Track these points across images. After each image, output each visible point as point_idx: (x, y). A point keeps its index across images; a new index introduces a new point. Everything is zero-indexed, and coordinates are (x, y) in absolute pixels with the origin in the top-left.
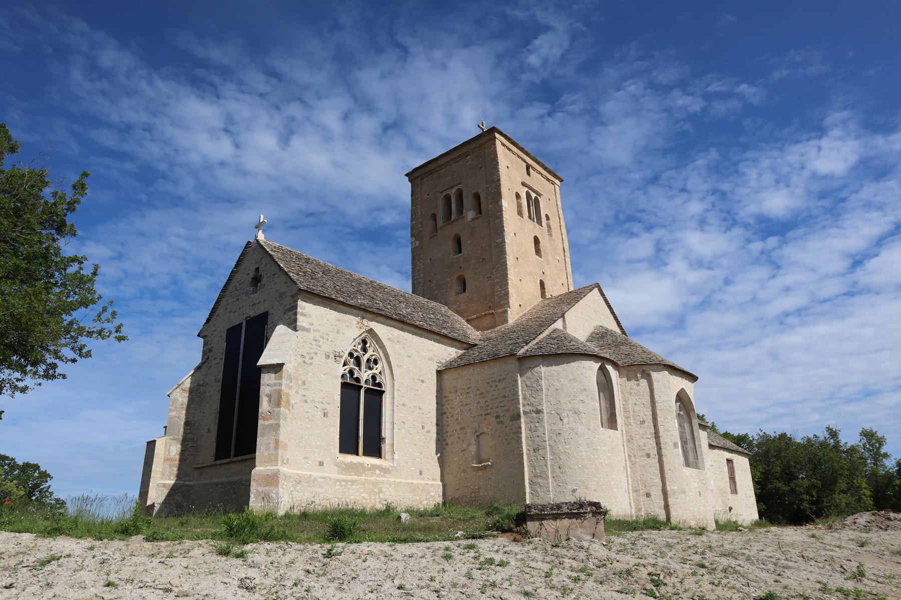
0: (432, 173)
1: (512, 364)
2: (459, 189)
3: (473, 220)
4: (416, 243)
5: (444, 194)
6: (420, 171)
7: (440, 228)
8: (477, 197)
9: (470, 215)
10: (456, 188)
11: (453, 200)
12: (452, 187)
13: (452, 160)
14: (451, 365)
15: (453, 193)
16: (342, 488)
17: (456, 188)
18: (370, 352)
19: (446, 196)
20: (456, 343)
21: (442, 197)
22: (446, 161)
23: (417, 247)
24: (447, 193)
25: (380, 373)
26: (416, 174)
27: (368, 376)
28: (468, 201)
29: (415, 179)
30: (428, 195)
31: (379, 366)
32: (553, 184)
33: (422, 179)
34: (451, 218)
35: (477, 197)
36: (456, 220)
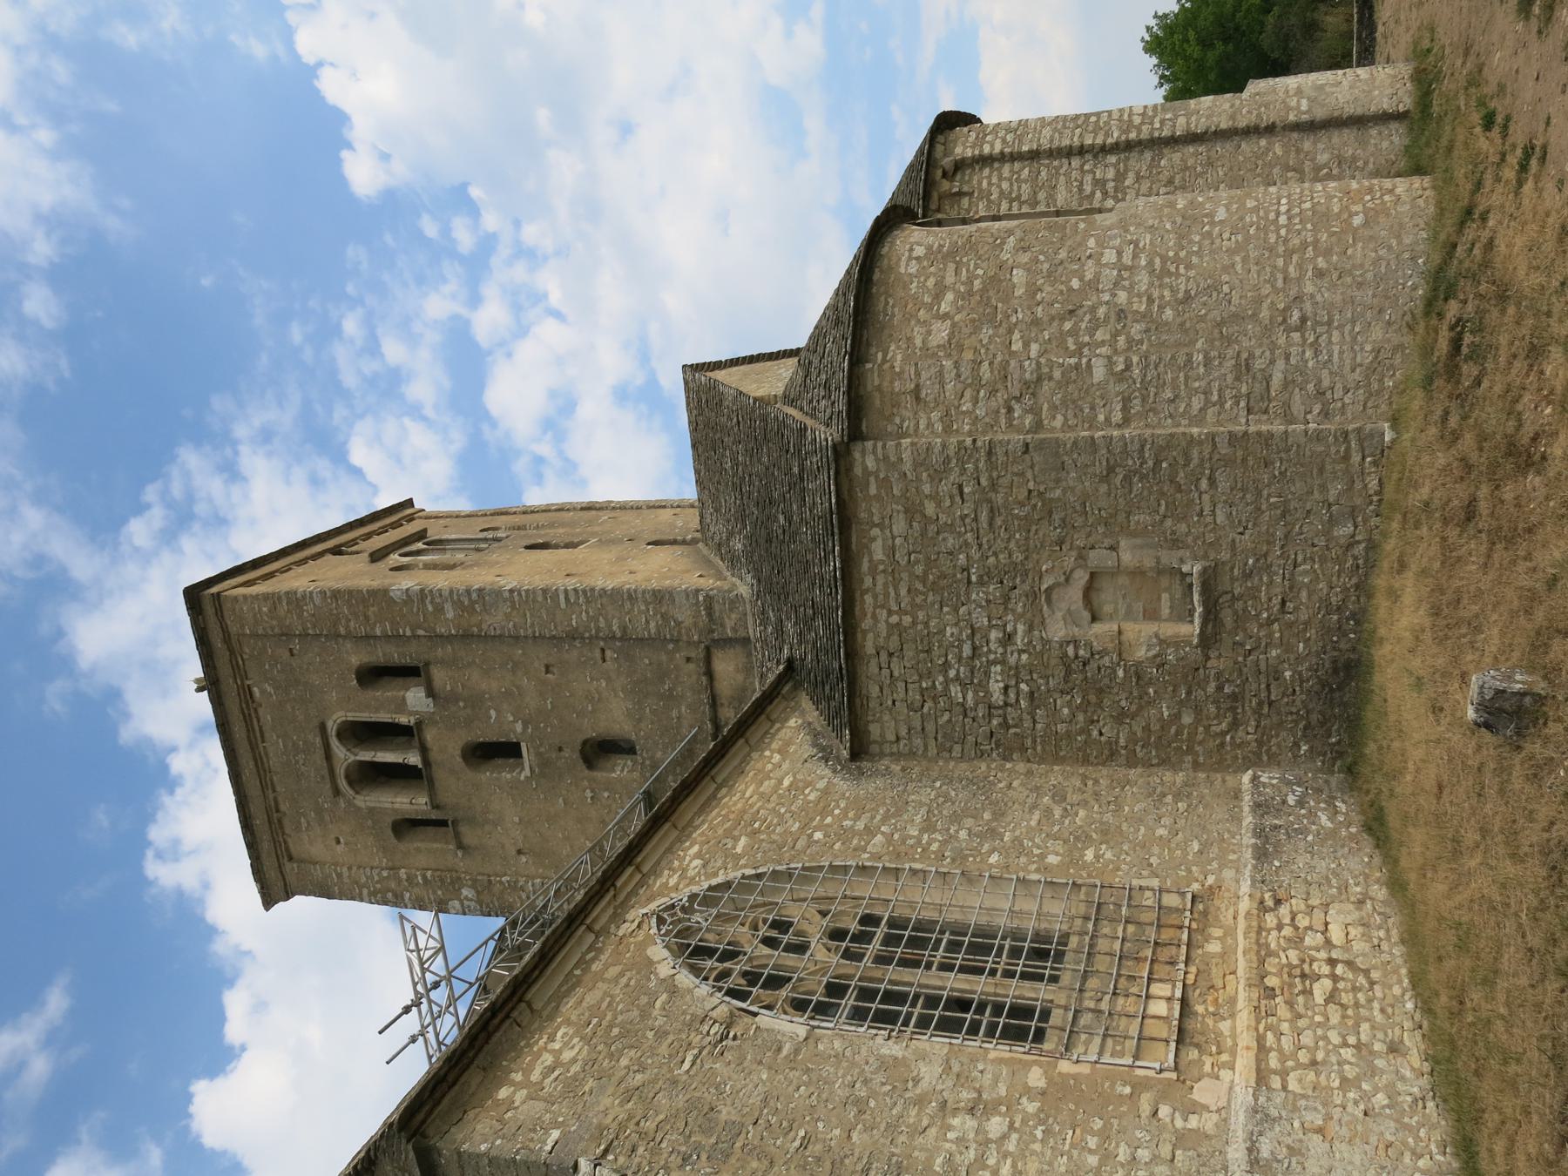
0: (280, 821)
1: (866, 459)
2: (339, 735)
3: (431, 693)
4: (466, 898)
5: (343, 784)
6: (264, 856)
7: (436, 807)
8: (372, 675)
9: (416, 698)
10: (334, 743)
11: (366, 756)
12: (328, 755)
13: (253, 747)
14: (838, 713)
15: (344, 756)
16: (1294, 1069)
17: (334, 743)
18: (739, 932)
19: (351, 783)
20: (775, 709)
21: (351, 792)
22: (252, 764)
23: (478, 893)
24: (342, 771)
25: (824, 914)
26: (272, 874)
27: (829, 950)
28: (377, 706)
29: (284, 879)
30: (338, 842)
31: (794, 913)
32: (413, 519)
33: (291, 858)
34: (415, 767)
35: (372, 675)
36: (424, 751)
